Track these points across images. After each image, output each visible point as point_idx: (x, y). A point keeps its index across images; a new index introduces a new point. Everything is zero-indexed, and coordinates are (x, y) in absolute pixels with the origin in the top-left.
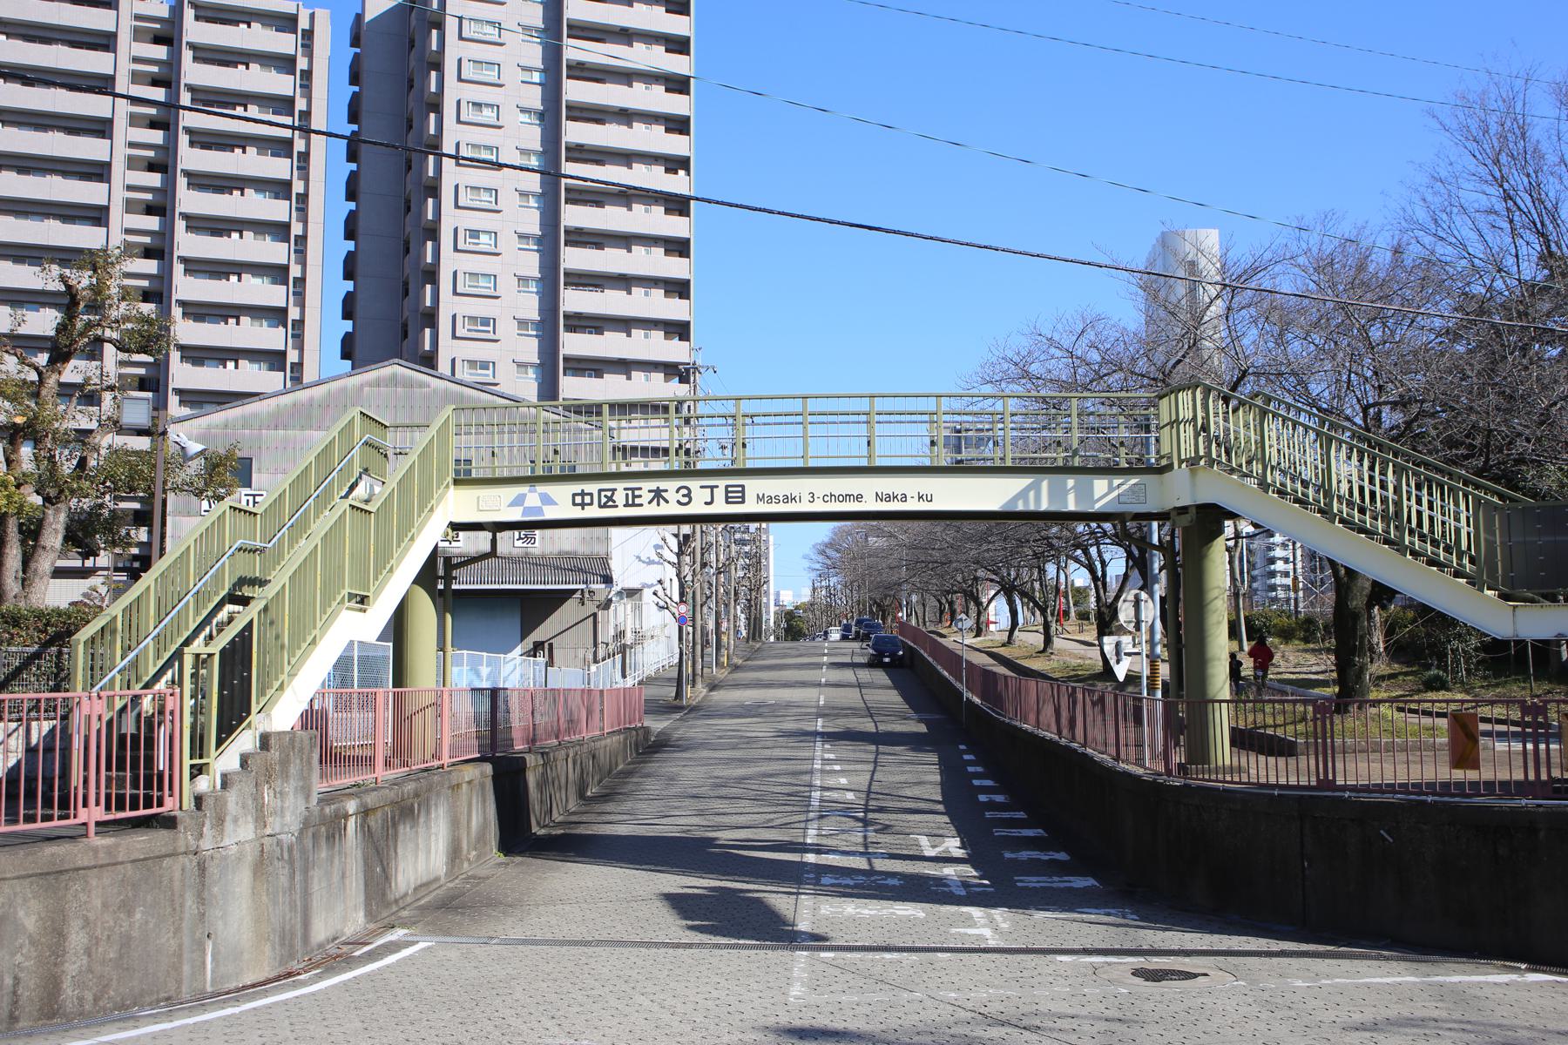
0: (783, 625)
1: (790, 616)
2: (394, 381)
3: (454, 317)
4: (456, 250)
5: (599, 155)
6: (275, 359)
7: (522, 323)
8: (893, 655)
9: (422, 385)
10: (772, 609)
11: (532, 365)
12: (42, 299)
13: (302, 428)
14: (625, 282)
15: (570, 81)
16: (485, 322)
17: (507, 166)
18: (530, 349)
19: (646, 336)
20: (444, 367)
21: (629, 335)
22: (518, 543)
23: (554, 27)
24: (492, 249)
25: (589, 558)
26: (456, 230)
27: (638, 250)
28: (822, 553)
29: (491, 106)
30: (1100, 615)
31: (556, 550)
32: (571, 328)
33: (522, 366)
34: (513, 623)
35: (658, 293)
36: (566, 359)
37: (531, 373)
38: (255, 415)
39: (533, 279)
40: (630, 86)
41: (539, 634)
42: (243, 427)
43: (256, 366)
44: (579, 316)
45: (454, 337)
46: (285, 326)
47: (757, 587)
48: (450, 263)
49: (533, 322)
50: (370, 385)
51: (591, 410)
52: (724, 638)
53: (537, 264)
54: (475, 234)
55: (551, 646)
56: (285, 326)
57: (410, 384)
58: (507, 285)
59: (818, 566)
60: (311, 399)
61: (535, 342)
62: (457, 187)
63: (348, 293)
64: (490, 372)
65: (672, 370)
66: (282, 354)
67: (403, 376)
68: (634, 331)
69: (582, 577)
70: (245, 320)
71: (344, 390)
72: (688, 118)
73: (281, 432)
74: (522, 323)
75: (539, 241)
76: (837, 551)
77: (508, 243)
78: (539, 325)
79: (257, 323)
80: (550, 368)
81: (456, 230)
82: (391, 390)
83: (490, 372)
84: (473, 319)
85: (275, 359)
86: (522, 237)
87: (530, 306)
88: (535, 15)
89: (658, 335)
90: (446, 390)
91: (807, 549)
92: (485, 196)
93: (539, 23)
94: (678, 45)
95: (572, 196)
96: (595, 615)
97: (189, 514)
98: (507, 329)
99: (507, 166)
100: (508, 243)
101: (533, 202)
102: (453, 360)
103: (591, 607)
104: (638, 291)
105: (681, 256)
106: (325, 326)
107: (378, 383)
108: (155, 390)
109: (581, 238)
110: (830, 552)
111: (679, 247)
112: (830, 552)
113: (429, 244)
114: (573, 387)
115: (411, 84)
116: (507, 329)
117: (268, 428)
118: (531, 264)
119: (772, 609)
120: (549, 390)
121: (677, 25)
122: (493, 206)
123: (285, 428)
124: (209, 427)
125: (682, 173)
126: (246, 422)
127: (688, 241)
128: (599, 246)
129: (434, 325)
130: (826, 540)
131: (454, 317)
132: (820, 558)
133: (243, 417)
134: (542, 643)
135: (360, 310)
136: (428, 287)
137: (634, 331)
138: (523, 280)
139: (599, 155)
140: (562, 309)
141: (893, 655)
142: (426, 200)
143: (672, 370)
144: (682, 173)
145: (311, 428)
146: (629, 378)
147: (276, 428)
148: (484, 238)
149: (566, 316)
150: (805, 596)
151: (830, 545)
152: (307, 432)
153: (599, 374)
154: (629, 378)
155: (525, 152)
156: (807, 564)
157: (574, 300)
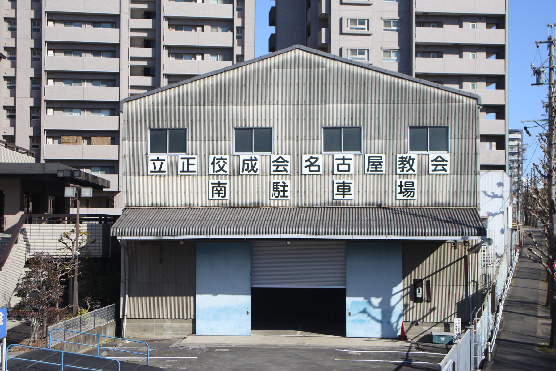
2: (296, 63)
6: (226, 53)
7: (387, 22)
9: (319, 65)
12: (83, 19)
13: (225, 104)
16: (362, 22)
18: (392, 40)
19: (473, 27)
20: (334, 51)
21: (461, 27)
22: (400, 197)
25: (461, 210)
30: (391, 91)
31: (432, 202)
32: (420, 24)
34: (398, 264)
36: (418, 45)
37: (394, 57)
38: (188, 94)
41: (417, 273)
42: (179, 104)
43: (215, 58)
45: (341, 33)
46: (232, 31)
50: (277, 66)
51: (440, 79)
55: (428, 283)
56: (232, 31)
57: (309, 65)
60: (231, 80)
61: (396, 34)
63: (272, 8)
64: (365, 56)
66: (231, 49)
67: (304, 59)
68: (464, 24)
69: (458, 229)
70: (207, 28)
71: (257, 71)
73: (208, 107)
74: (387, 22)
78: (398, 23)
79: (215, 30)
80: (406, 53)
82: (294, 70)
83: (365, 56)
84: (353, 21)
85: (226, 53)
90: (339, 68)
96: (466, 258)
97: (139, 174)
98: (376, 26)
103: (462, 251)
106: (258, 30)
107: (283, 65)
108: (153, 75)
114: (421, 65)
116: (376, 26)
117: (198, 104)
120: (405, 67)
123: (211, 104)
124: (153, 104)
126: (181, 101)
129: (327, 25)
131: (341, 20)
133: (179, 96)
134: (421, 280)
135: (279, 20)
136: (323, 30)
137: (464, 24)
142: (320, 30)
145: (231, 103)
146: (461, 57)
147: (204, 104)
152: (228, 107)
153: (440, 55)
154: (461, 57)
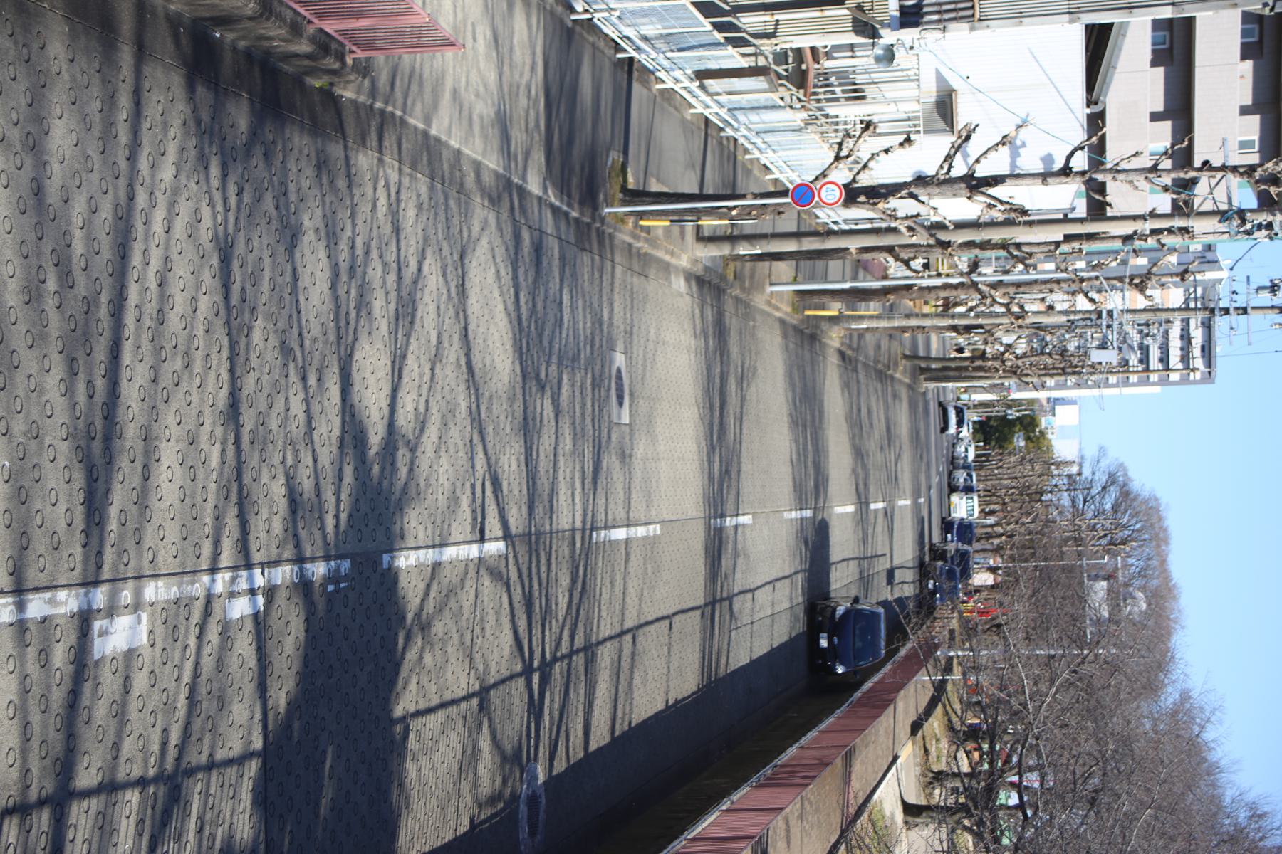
0: (1013, 414)
1: (1029, 424)
8: (834, 653)
10: (1042, 395)
28: (1112, 479)
40: (1154, 63)
47: (1069, 366)
76: (1115, 508)
96: (730, 110)
112: (1113, 493)
119: (1042, 395)
130: (1136, 486)
132: (1101, 478)
137: (1255, 120)
141: (834, 653)
146: (1244, 111)
150: (1063, 447)
151: (1126, 493)
154: (1244, 111)
156: (1091, 452)
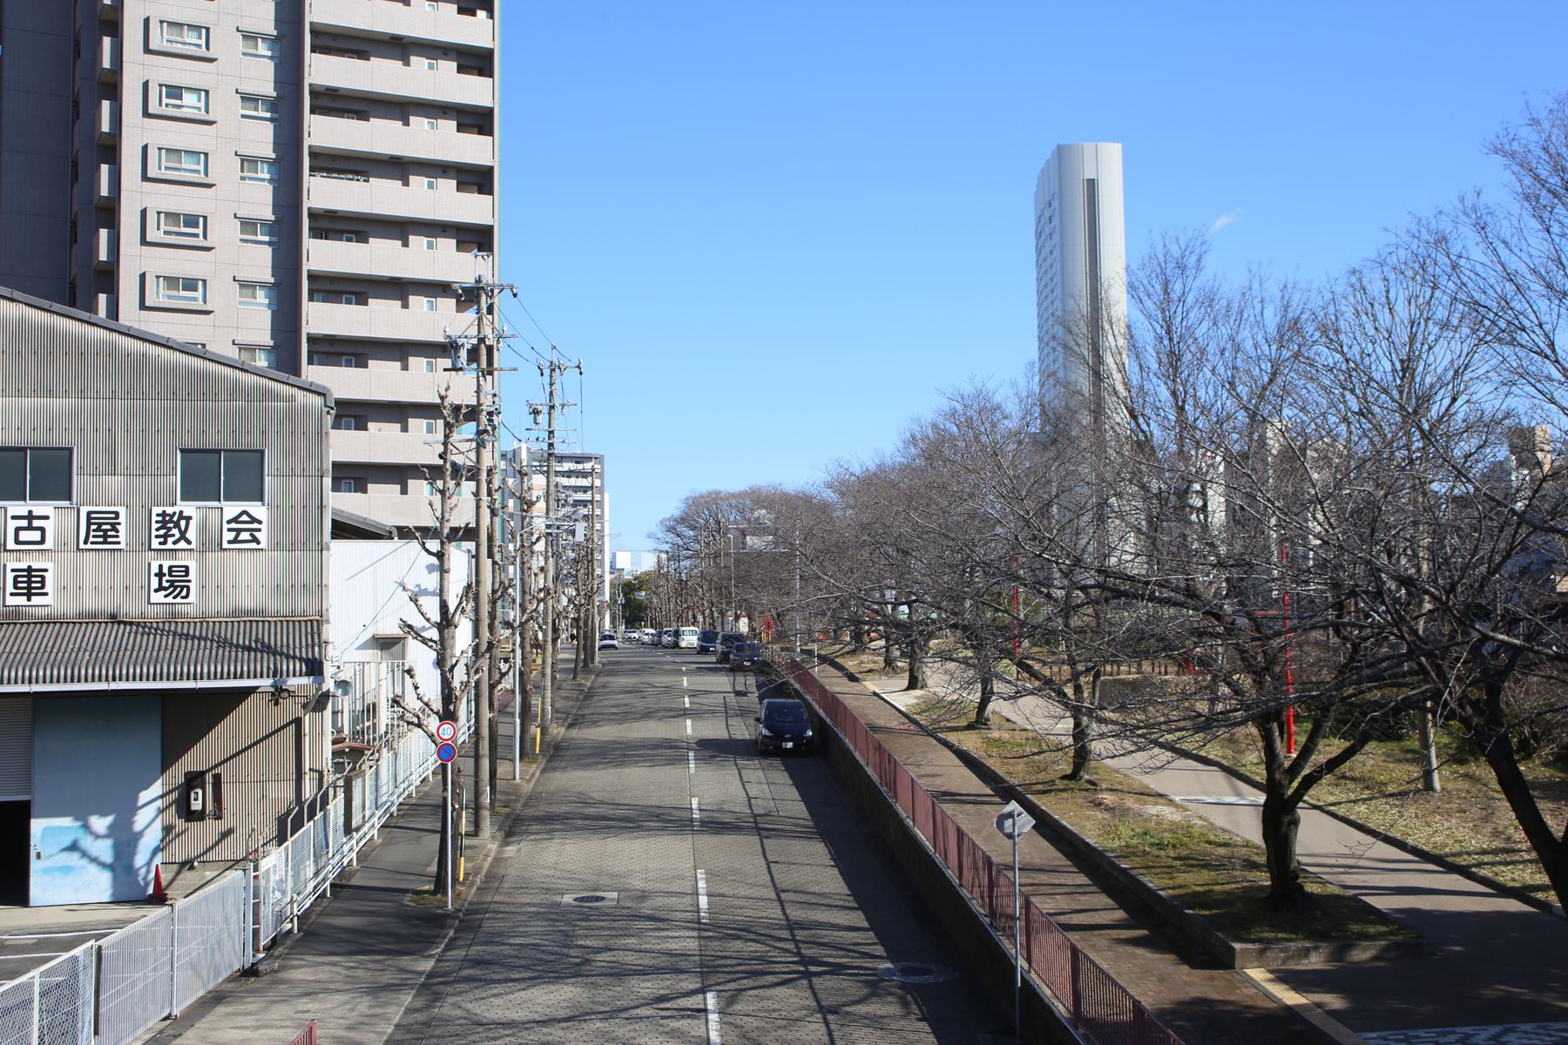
0: (621, 600)
3: (144, 213)
4: (146, 114)
5: (355, 289)
7: (248, 225)
10: (608, 578)
11: (263, 285)
14: (399, 168)
15: (315, 117)
17: (217, 843)
23: (292, 35)
24: (202, 115)
26: (146, 85)
27: (419, 123)
28: (671, 529)
29: (195, 28)
32: (318, 233)
33: (247, 286)
35: (448, 185)
37: (262, 297)
39: (264, 160)
44: (331, 215)
47: (587, 557)
48: (136, 133)
49: (264, 223)
52: (536, 701)
53: (270, 264)
54: (175, 92)
58: (224, 169)
59: (666, 547)
61: (267, 252)
62: (143, 277)
64: (200, 231)
65: (469, 296)
72: (490, 52)
75: (274, 41)
76: (693, 528)
77: (226, 108)
78: (272, 228)
81: (146, 85)
84: (172, 217)
86: (247, 99)
87: (260, 200)
88: (265, 19)
89: (448, 244)
91: (653, 526)
92: (191, 37)
93: (268, 89)
94: (476, 61)
95: (321, 42)
99: (217, 843)
100: (226, 108)
101: (263, 49)
102: (143, 277)
104: (418, 182)
105: (480, 133)
109: (334, 225)
110: (682, 529)
111: (476, 120)
112: (682, 529)
113: (105, 168)
115: (79, 49)
116: (224, 231)
118: (261, 138)
121: (475, 31)
122: (202, 52)
125: (481, 14)
127: (490, 111)
128: (363, 115)
130: (677, 513)
131: (144, 213)
132: (671, 537)
138: (248, 162)
139: (355, 289)
140: (306, 330)
143: (469, 296)
144: (481, 14)
146: (405, 306)
148: (189, 98)
149: (313, 155)
150: (648, 563)
154: (405, 306)
155: (249, 348)
156: (652, 544)
157: (323, 193)
